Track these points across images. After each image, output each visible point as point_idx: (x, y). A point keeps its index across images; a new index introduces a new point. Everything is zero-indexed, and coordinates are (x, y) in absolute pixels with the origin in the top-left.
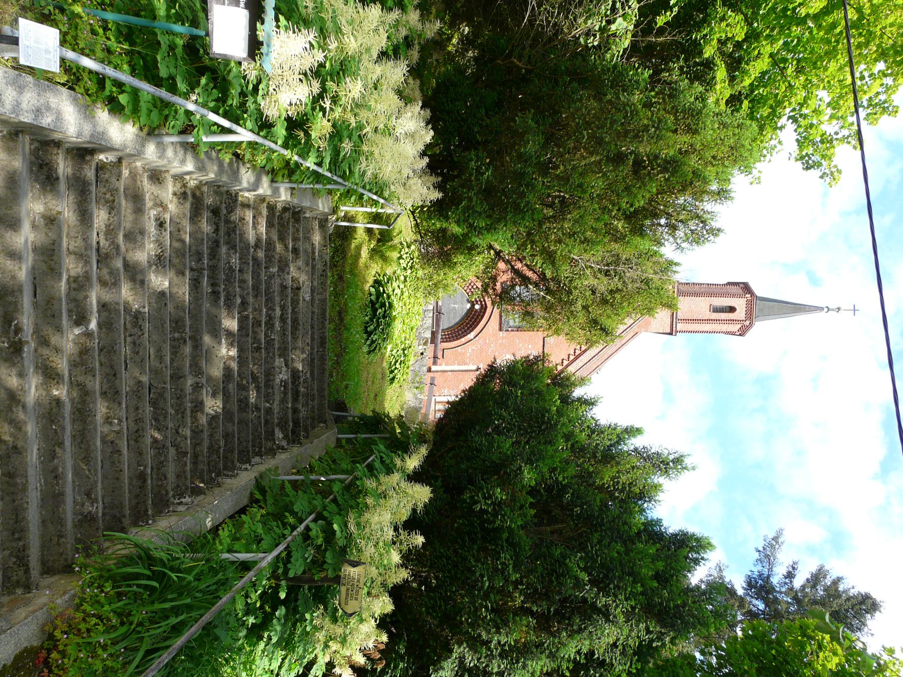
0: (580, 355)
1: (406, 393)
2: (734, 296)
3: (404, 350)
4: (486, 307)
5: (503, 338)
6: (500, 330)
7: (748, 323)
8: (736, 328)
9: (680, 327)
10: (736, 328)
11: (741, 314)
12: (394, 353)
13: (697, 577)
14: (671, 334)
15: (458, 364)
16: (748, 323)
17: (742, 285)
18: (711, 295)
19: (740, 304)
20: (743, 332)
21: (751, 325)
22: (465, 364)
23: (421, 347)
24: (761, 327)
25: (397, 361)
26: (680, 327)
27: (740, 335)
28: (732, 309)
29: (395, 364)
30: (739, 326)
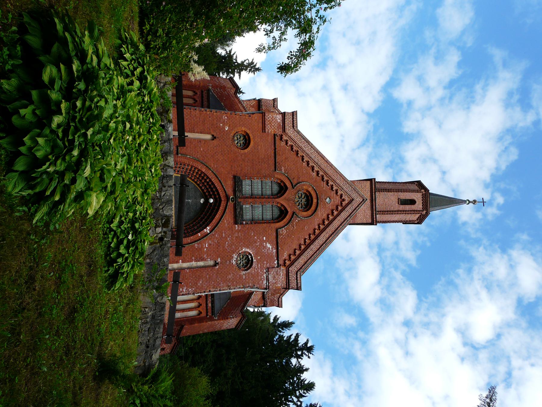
0: (310, 245)
1: (141, 297)
2: (413, 191)
3: (133, 222)
4: (221, 201)
5: (238, 231)
6: (236, 223)
7: (425, 212)
8: (415, 217)
9: (379, 217)
10: (415, 217)
11: (419, 206)
12: (114, 226)
13: (306, 382)
14: (372, 224)
15: (196, 261)
16: (425, 212)
17: (416, 183)
18: (398, 191)
19: (418, 197)
20: (420, 221)
21: (427, 214)
22: (202, 259)
23: (159, 230)
24: (435, 214)
25: (120, 242)
26: (379, 217)
27: (418, 223)
28: (412, 202)
29: (117, 247)
30: (418, 216)
